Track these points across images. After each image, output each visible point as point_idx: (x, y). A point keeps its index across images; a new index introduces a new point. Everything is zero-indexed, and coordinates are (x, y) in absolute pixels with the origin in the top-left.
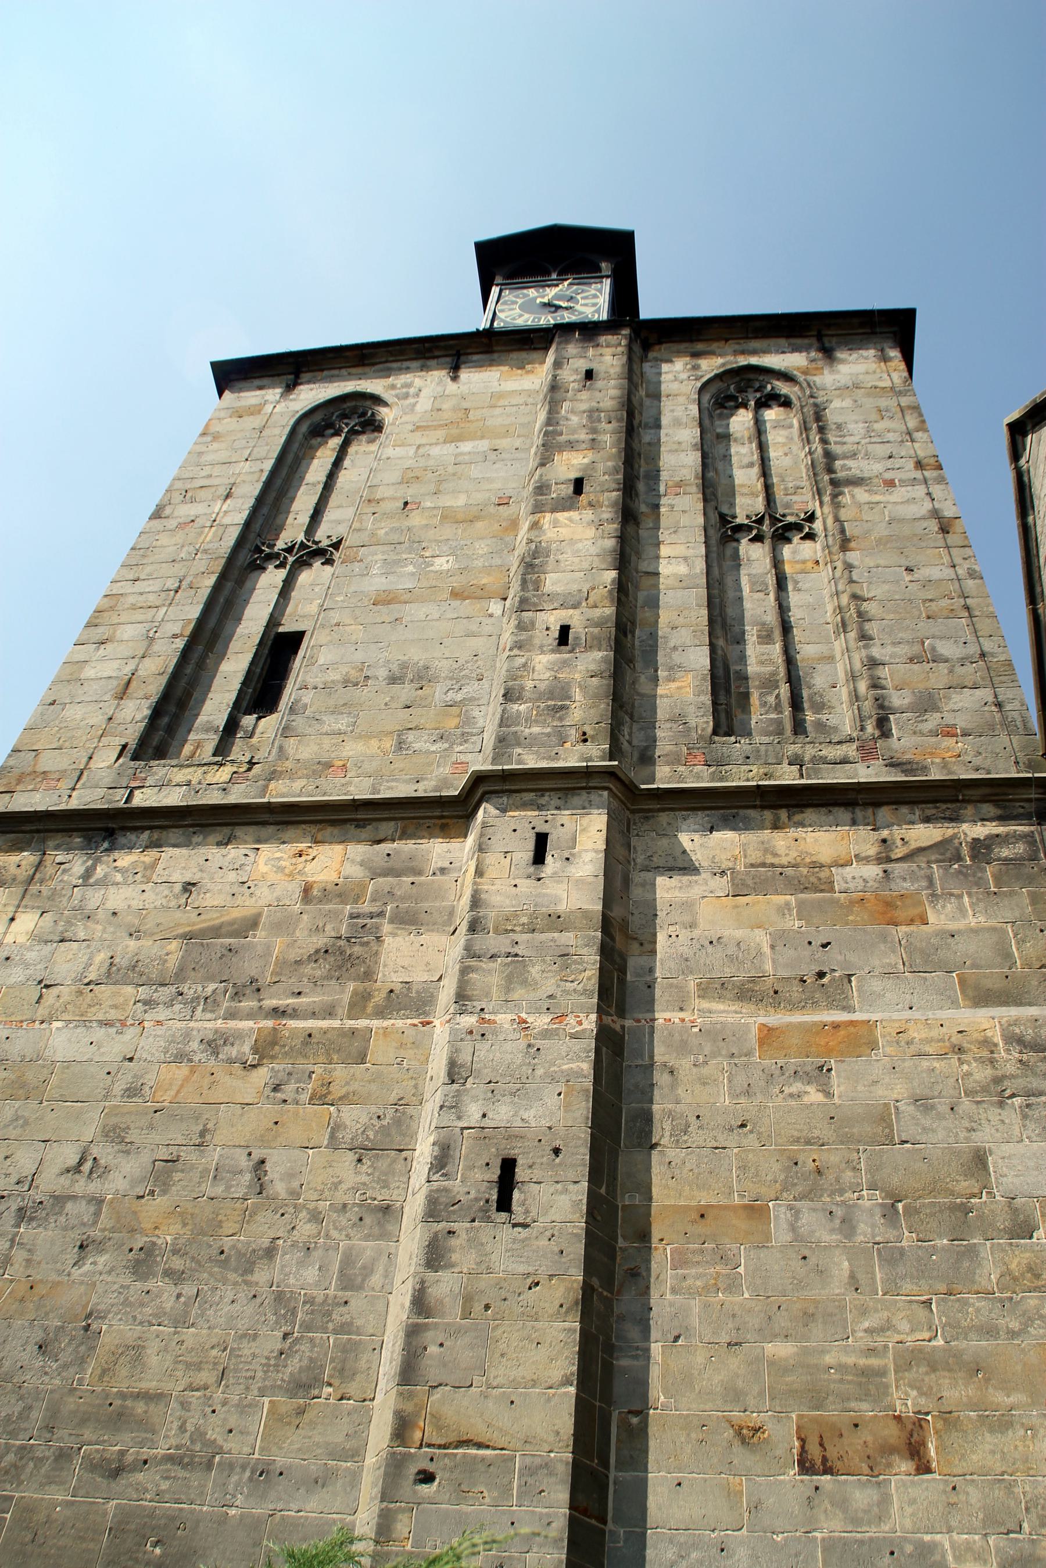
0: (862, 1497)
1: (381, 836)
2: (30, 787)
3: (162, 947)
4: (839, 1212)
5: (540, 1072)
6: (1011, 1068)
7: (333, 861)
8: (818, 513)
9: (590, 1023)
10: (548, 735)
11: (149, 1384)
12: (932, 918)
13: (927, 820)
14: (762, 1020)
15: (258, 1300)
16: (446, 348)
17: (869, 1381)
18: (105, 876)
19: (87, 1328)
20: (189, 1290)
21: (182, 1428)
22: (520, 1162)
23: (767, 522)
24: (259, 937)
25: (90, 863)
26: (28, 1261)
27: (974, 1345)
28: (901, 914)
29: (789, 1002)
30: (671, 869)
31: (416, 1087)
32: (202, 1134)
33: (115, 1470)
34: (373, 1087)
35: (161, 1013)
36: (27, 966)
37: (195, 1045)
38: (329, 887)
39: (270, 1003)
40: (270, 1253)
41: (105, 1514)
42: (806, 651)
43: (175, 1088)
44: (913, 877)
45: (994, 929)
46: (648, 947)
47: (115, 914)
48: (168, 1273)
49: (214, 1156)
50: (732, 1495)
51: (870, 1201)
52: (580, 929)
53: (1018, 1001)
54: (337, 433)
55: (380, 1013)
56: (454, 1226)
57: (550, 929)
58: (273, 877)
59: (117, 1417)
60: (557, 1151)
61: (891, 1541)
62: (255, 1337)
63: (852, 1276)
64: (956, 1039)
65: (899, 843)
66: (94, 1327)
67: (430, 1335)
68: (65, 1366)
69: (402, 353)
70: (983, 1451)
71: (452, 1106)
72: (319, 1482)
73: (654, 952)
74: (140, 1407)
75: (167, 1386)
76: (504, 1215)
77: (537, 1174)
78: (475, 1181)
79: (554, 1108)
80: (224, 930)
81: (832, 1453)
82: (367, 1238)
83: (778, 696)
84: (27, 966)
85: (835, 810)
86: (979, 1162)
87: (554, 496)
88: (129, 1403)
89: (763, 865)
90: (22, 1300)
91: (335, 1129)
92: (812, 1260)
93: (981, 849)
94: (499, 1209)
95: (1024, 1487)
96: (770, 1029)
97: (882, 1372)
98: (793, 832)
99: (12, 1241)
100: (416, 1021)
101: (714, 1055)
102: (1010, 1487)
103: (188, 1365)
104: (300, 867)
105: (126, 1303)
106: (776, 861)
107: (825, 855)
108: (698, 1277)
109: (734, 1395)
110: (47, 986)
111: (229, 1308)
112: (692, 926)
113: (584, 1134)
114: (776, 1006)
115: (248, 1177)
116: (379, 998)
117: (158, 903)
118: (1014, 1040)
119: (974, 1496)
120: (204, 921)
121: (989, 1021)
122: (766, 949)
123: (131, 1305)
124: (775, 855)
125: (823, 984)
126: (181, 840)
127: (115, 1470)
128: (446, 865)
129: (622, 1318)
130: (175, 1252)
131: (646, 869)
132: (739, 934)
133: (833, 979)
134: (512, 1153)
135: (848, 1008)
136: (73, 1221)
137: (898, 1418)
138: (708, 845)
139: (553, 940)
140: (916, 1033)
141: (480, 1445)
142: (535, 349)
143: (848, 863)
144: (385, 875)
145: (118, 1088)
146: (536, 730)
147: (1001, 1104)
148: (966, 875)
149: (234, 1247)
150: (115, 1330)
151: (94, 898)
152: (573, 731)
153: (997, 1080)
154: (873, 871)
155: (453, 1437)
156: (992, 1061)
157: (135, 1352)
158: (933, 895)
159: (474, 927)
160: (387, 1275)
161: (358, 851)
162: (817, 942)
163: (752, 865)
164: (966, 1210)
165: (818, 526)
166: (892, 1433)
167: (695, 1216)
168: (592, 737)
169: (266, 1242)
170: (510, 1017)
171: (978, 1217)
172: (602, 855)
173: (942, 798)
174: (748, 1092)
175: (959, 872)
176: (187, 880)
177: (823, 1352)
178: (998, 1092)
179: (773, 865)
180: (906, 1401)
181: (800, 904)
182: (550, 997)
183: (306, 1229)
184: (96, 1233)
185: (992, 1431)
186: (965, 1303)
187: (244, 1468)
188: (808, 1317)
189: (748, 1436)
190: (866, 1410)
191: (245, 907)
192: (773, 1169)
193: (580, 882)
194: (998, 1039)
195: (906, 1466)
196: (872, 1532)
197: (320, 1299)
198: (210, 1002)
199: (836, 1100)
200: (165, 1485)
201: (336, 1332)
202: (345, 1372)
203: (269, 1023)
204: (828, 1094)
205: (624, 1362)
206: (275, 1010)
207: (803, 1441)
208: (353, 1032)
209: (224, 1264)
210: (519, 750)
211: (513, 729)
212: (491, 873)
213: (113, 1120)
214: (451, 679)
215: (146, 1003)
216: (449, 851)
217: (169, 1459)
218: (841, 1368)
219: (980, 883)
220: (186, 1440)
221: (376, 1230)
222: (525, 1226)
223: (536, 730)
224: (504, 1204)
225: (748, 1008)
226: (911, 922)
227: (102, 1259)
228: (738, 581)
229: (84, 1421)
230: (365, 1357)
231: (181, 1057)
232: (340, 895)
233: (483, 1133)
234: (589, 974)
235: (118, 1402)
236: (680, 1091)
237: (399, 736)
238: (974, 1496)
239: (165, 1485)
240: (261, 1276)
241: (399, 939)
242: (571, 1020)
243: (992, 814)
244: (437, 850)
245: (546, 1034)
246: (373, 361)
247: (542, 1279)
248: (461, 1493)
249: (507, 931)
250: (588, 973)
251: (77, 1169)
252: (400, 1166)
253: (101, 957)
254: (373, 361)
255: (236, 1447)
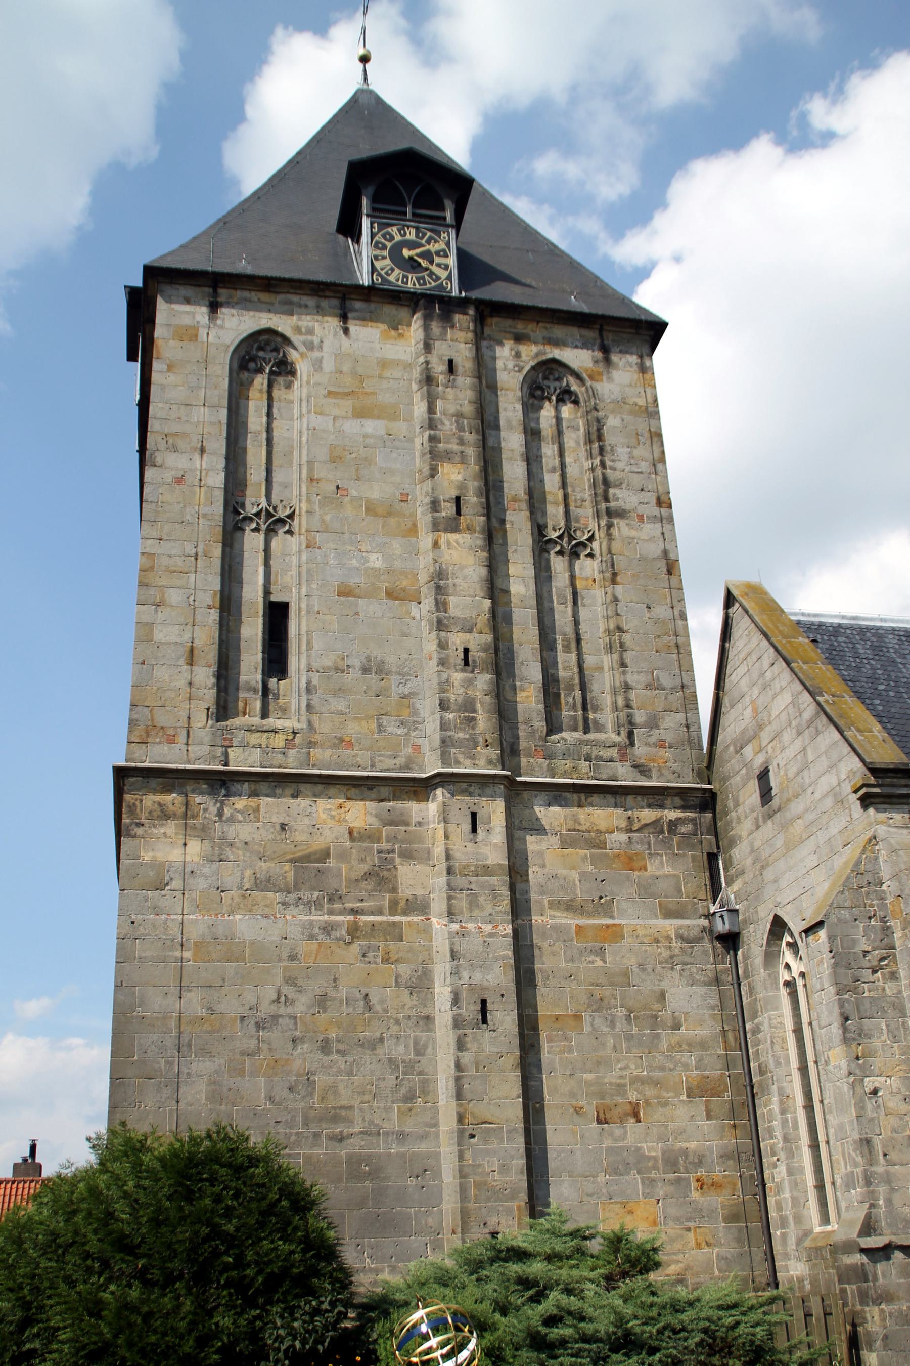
0: (618, 1132)
1: (383, 797)
2: (158, 740)
3: (281, 868)
4: (609, 1018)
5: (491, 956)
6: (677, 951)
7: (360, 813)
8: (597, 536)
9: (509, 929)
10: (468, 740)
11: (344, 1103)
12: (649, 868)
13: (649, 806)
14: (577, 922)
15: (382, 1062)
16: (334, 292)
17: (620, 1088)
18: (232, 815)
19: (308, 1079)
20: (350, 1059)
21: (363, 1119)
22: (488, 1001)
23: (566, 539)
24: (332, 863)
25: (218, 805)
26: (270, 1049)
27: (658, 1074)
28: (636, 865)
29: (588, 913)
30: (531, 830)
31: (429, 954)
32: (335, 980)
33: (340, 1139)
34: (410, 955)
35: (293, 911)
36: (206, 877)
37: (316, 930)
38: (362, 831)
39: (349, 905)
40: (381, 1040)
41: (342, 1157)
42: (590, 660)
43: (314, 955)
44: (640, 841)
45: (675, 876)
46: (524, 878)
47: (246, 843)
48: (338, 1052)
49: (343, 992)
50: (574, 1133)
51: (621, 1012)
52: (499, 876)
53: (682, 917)
54: (260, 371)
55: (405, 913)
56: (466, 1031)
57: (485, 875)
58: (331, 823)
59: (335, 1117)
60: (502, 995)
61: (627, 1147)
62: (384, 1079)
63: (614, 1046)
64: (656, 935)
65: (636, 820)
66: (311, 1078)
67: (464, 1080)
68: (304, 1097)
69: (300, 288)
70: (659, 1114)
71: (455, 973)
72: (424, 1137)
73: (527, 881)
74: (343, 1113)
75: (352, 1103)
76: (485, 1026)
77: (496, 1007)
78: (471, 1010)
79: (498, 976)
80: (312, 858)
81: (608, 1116)
82: (422, 1031)
83: (574, 697)
84: (206, 877)
85: (607, 796)
86: (662, 996)
87: (444, 514)
88: (338, 1111)
89: (574, 830)
90: (273, 1068)
91: (397, 977)
92: (600, 1039)
93: (673, 825)
94: (483, 1023)
95: (671, 1126)
96: (580, 927)
97: (625, 1085)
98: (588, 810)
99: (259, 1040)
100: (423, 918)
101: (558, 940)
102: (666, 1127)
103: (359, 1093)
104: (343, 816)
105: (322, 1066)
106: (580, 828)
107: (603, 826)
108: (557, 1046)
109: (573, 1095)
110: (223, 891)
111: (370, 1067)
112: (544, 866)
113: (513, 987)
114: (582, 914)
115: (362, 1003)
116: (402, 904)
117: (270, 837)
118: (680, 937)
119: (655, 1130)
120: (300, 851)
121: (670, 926)
122: (577, 882)
123: (325, 1067)
124: (580, 824)
125: (602, 905)
126: (268, 792)
127: (340, 1139)
128: (420, 820)
129: (530, 1065)
130: (339, 1041)
131: (520, 829)
132: (565, 872)
133: (606, 901)
134: (485, 997)
135: (612, 917)
136: (285, 1028)
137: (630, 1103)
138: (551, 815)
139: (487, 881)
140: (641, 932)
141: (490, 1123)
142: (402, 305)
143: (613, 832)
144: (390, 825)
145: (285, 955)
146: (461, 735)
147: (672, 969)
148: (665, 843)
149: (364, 1038)
150: (321, 1079)
151: (232, 831)
152: (480, 739)
153: (672, 957)
154: (623, 837)
155: (480, 1121)
156: (670, 947)
157: (333, 1089)
158: (650, 854)
159: (450, 871)
160: (434, 1048)
161: (372, 806)
162: (599, 880)
163: (569, 830)
164: (656, 1017)
165: (595, 545)
166: (628, 1108)
167: (554, 1019)
168: (491, 744)
169: (378, 1034)
170: (474, 925)
171: (661, 1021)
172: (504, 829)
173: (656, 796)
174: (572, 960)
175: (662, 840)
176: (282, 821)
177: (604, 1077)
178: (671, 962)
179: (579, 831)
180: (633, 1096)
181: (592, 855)
182: (490, 915)
183: (395, 1028)
184: (298, 1034)
185: (662, 1107)
186: (654, 1057)
187: (393, 1133)
188: (598, 1063)
189: (578, 1111)
190: (620, 1100)
191: (318, 843)
192: (584, 998)
193: (496, 845)
194: (673, 936)
195: (633, 1120)
196: (621, 1144)
197: (408, 1061)
198: (318, 904)
199: (608, 965)
200: (363, 1143)
201: (418, 1075)
202: (425, 1092)
203: (351, 918)
204: (605, 962)
205: (532, 1083)
206: (352, 910)
207: (598, 1112)
208: (394, 923)
209: (362, 1046)
210: (453, 750)
211: (449, 733)
212: (452, 838)
213: (288, 974)
214: (399, 674)
215: (283, 904)
216: (420, 810)
217: (362, 1132)
218: (611, 1084)
219: (671, 848)
220: (366, 1124)
221: (425, 1027)
222: (494, 1031)
223: (461, 735)
224: (485, 1021)
225: (570, 915)
226: (640, 870)
227: (305, 1046)
228: (550, 591)
229: (321, 1119)
230: (432, 1085)
231: (312, 937)
232: (369, 837)
233: (472, 988)
234: (506, 903)
235: (333, 1111)
236: (544, 958)
237: (378, 719)
238: (655, 1130)
239: (363, 1143)
240: (379, 1051)
241: (405, 867)
242: (500, 928)
243: (678, 805)
244: (413, 808)
245: (491, 935)
246: (278, 290)
247: (504, 1054)
248: (486, 1141)
249: (465, 875)
250: (505, 902)
251: (277, 1001)
252: (429, 996)
253: (248, 873)
254: (278, 290)
255: (387, 1126)
